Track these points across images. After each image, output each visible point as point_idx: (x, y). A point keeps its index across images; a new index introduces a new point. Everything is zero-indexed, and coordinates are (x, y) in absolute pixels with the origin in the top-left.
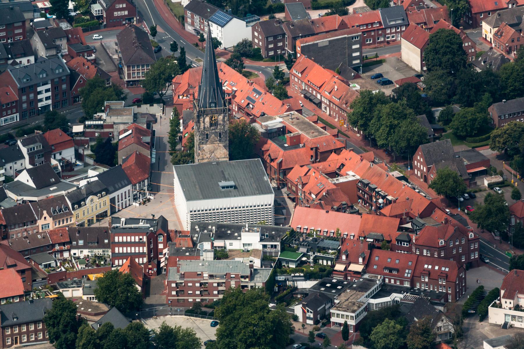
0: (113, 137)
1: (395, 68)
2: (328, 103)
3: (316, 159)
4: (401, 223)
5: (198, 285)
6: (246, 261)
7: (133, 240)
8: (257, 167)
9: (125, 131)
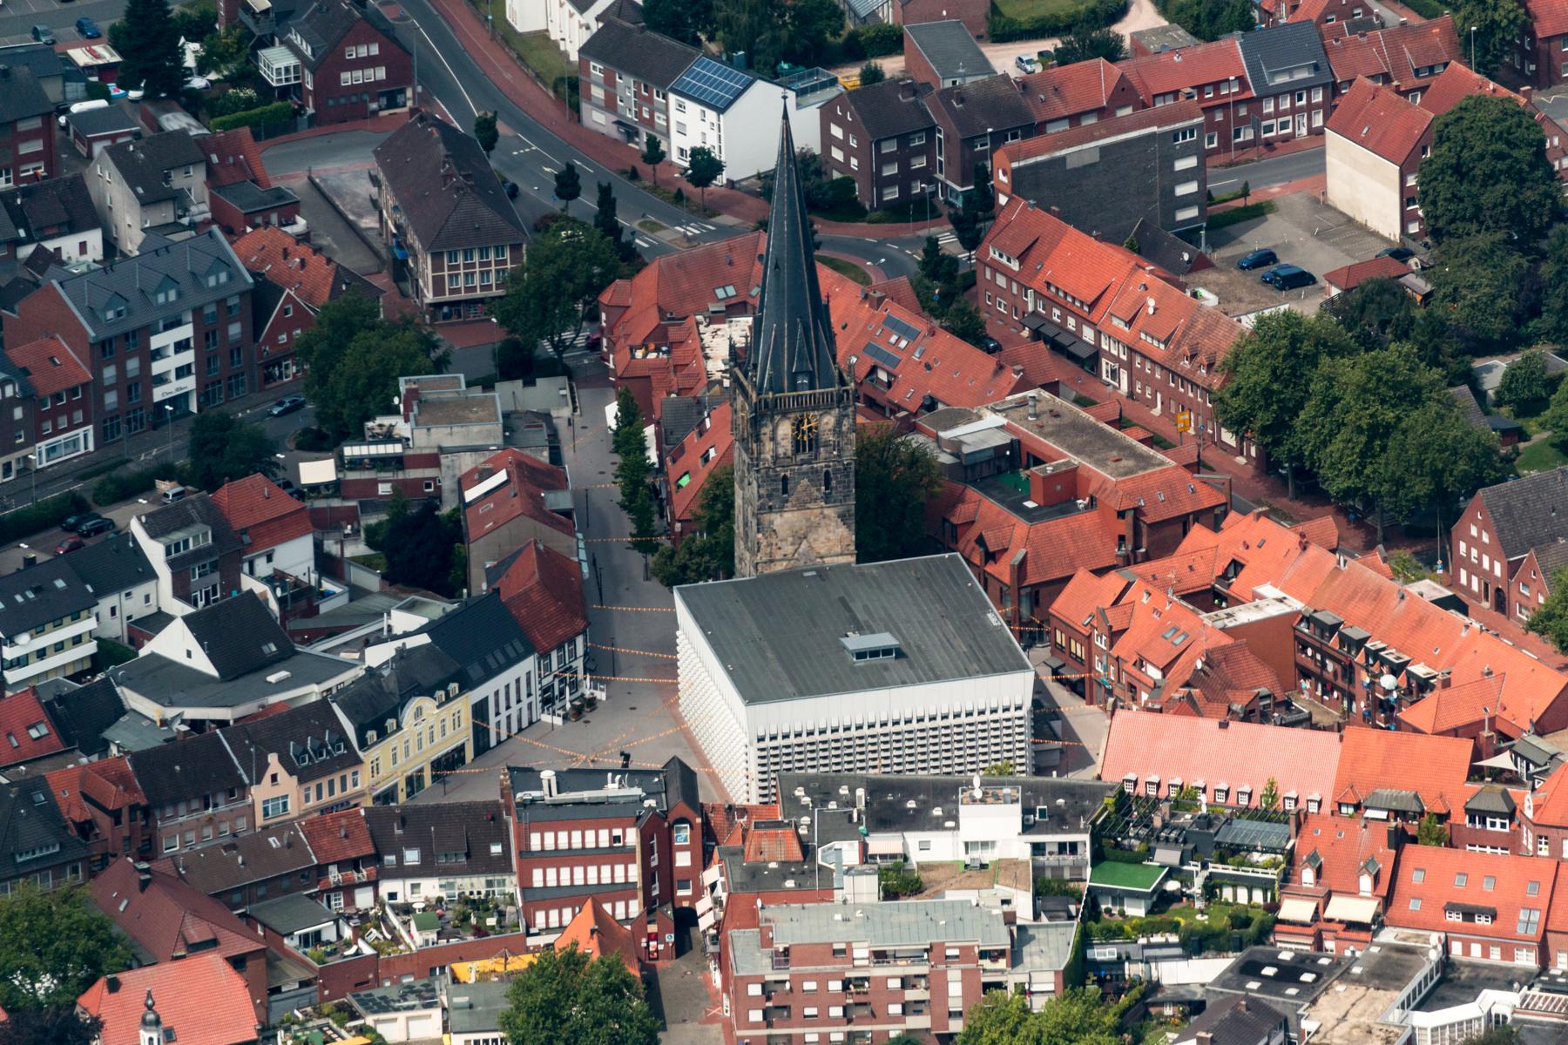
0: (438, 494)
1: (1310, 230)
2: (1124, 358)
3: (1137, 546)
4: (1477, 754)
5: (835, 986)
6: (989, 898)
7: (590, 844)
8: (957, 584)
9: (486, 474)
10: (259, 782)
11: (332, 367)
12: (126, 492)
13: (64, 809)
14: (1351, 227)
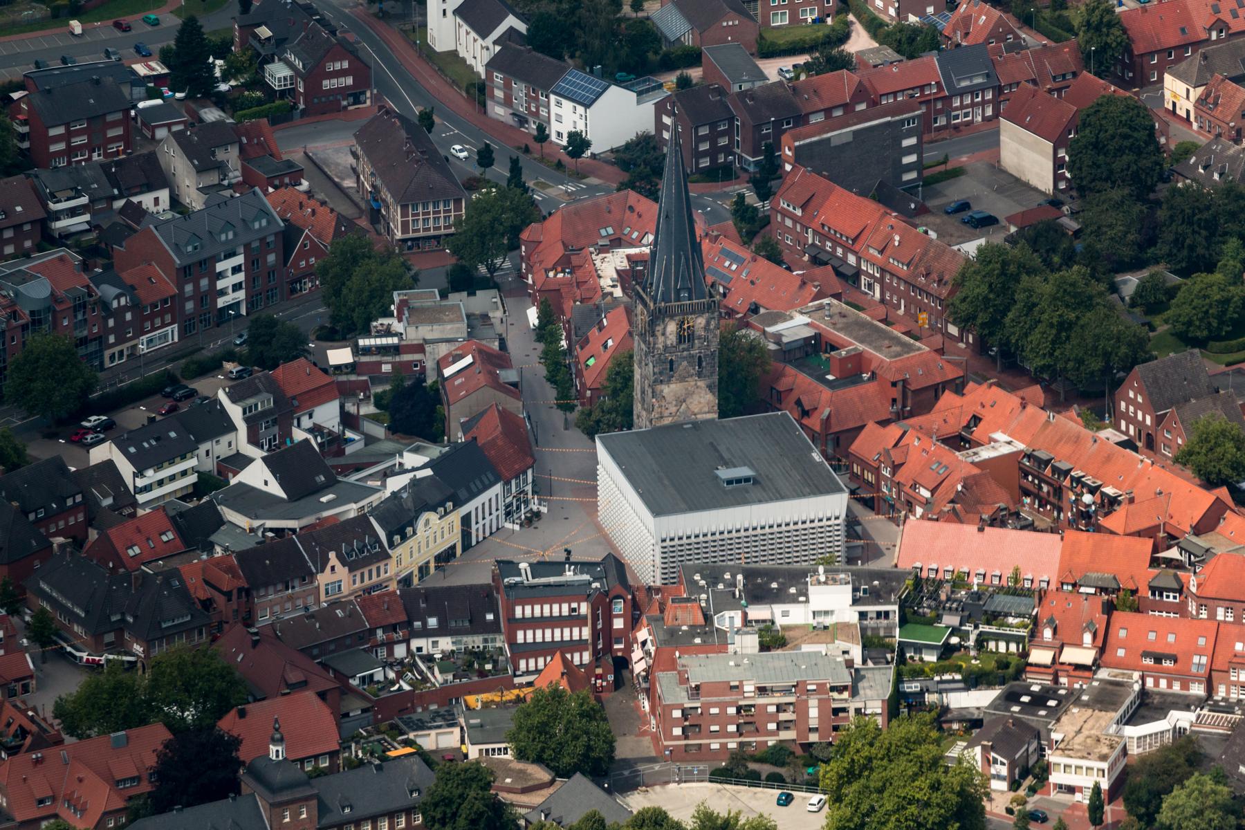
3: (904, 406)
4: (1156, 549)
5: (732, 711)
10: (322, 571)
11: (344, 284)
12: (209, 368)
13: (192, 591)
14: (1016, 186)
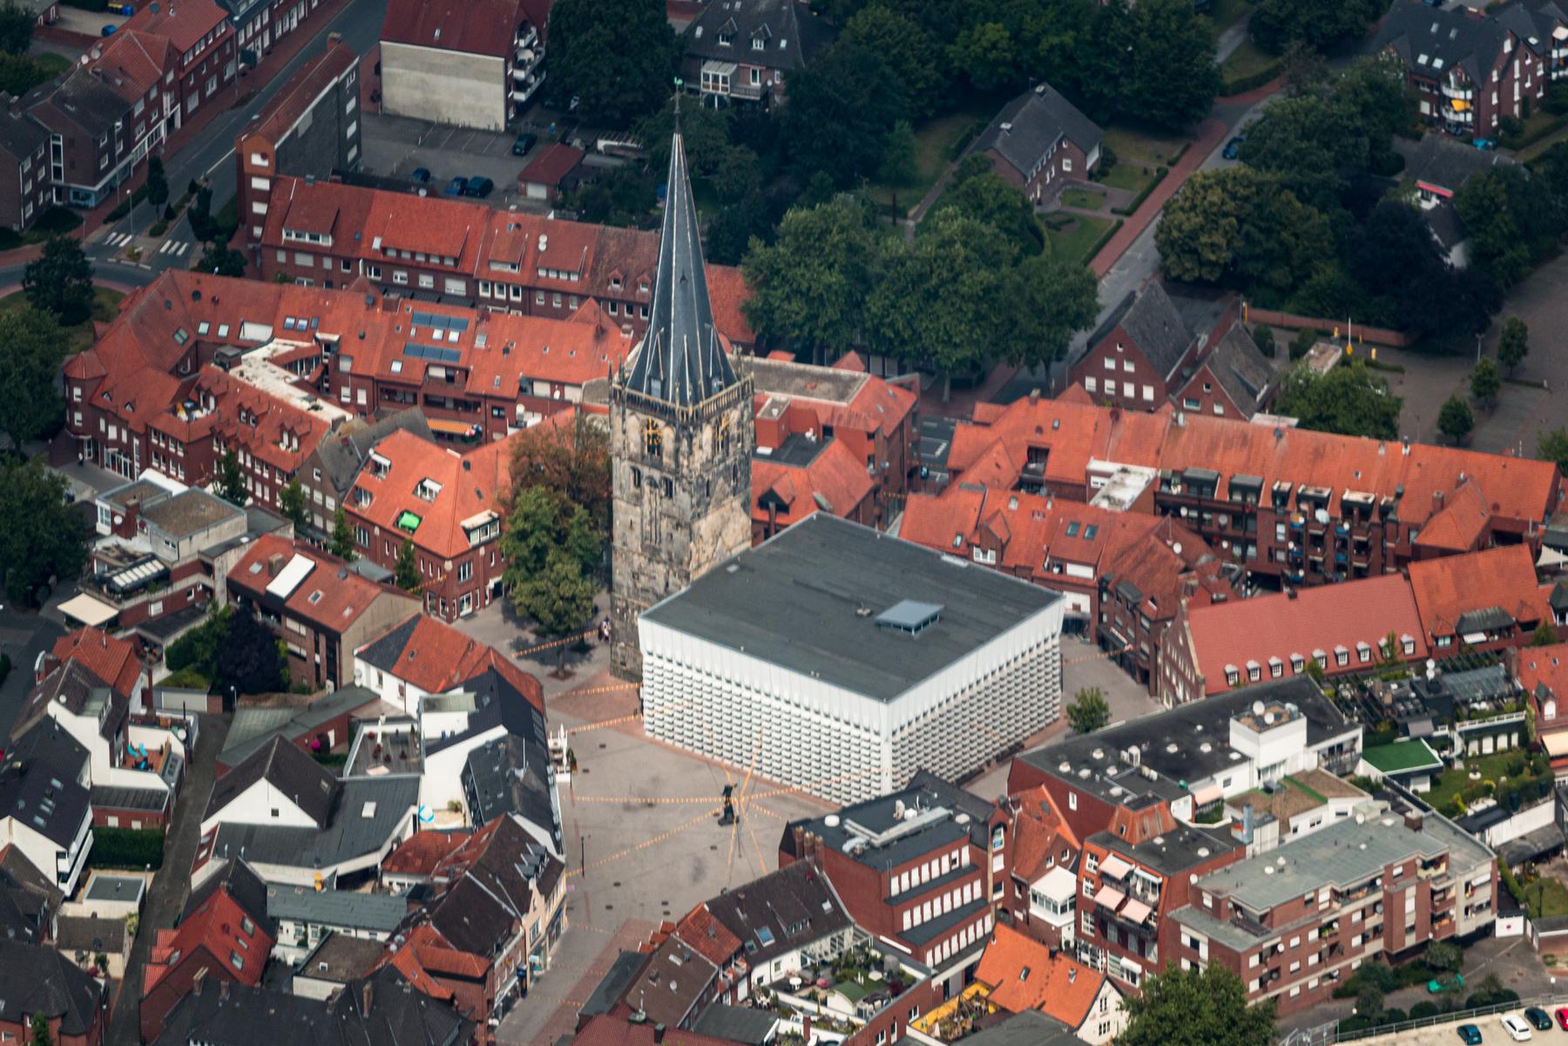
5: (1313, 935)
